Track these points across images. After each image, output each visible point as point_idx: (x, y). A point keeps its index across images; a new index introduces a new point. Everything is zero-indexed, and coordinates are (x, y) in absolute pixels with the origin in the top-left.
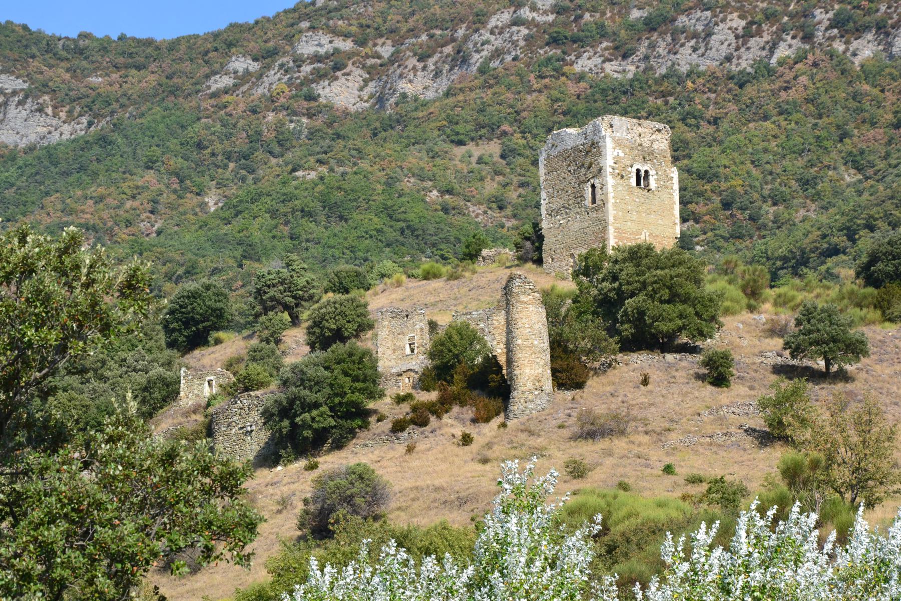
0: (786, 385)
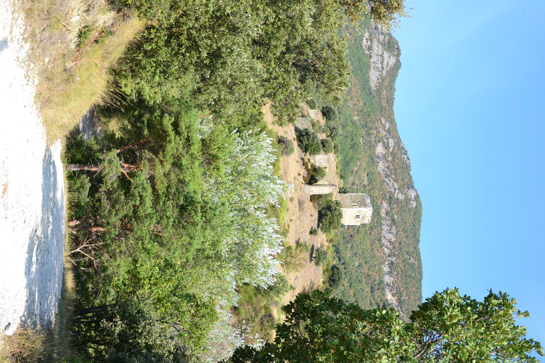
0: (310, 248)
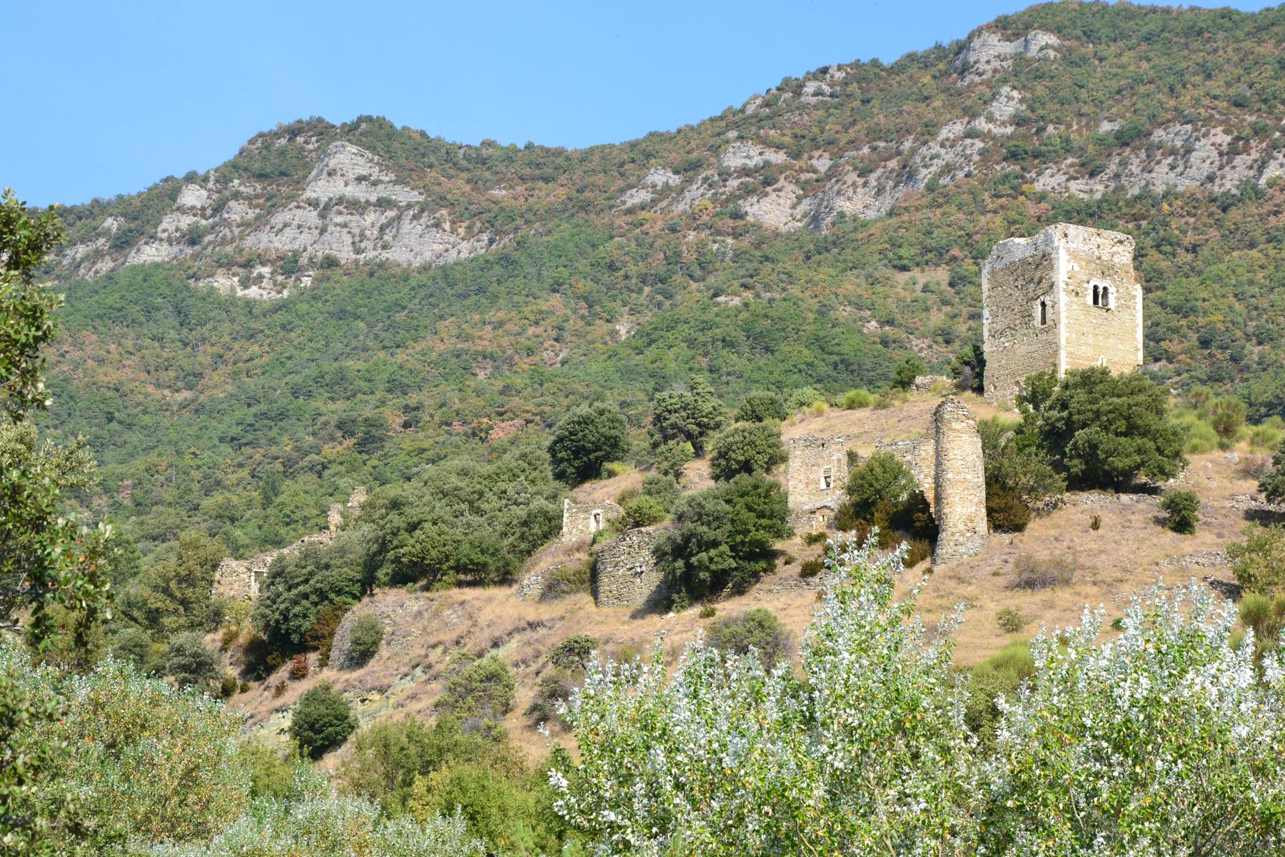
0: (1258, 531)
